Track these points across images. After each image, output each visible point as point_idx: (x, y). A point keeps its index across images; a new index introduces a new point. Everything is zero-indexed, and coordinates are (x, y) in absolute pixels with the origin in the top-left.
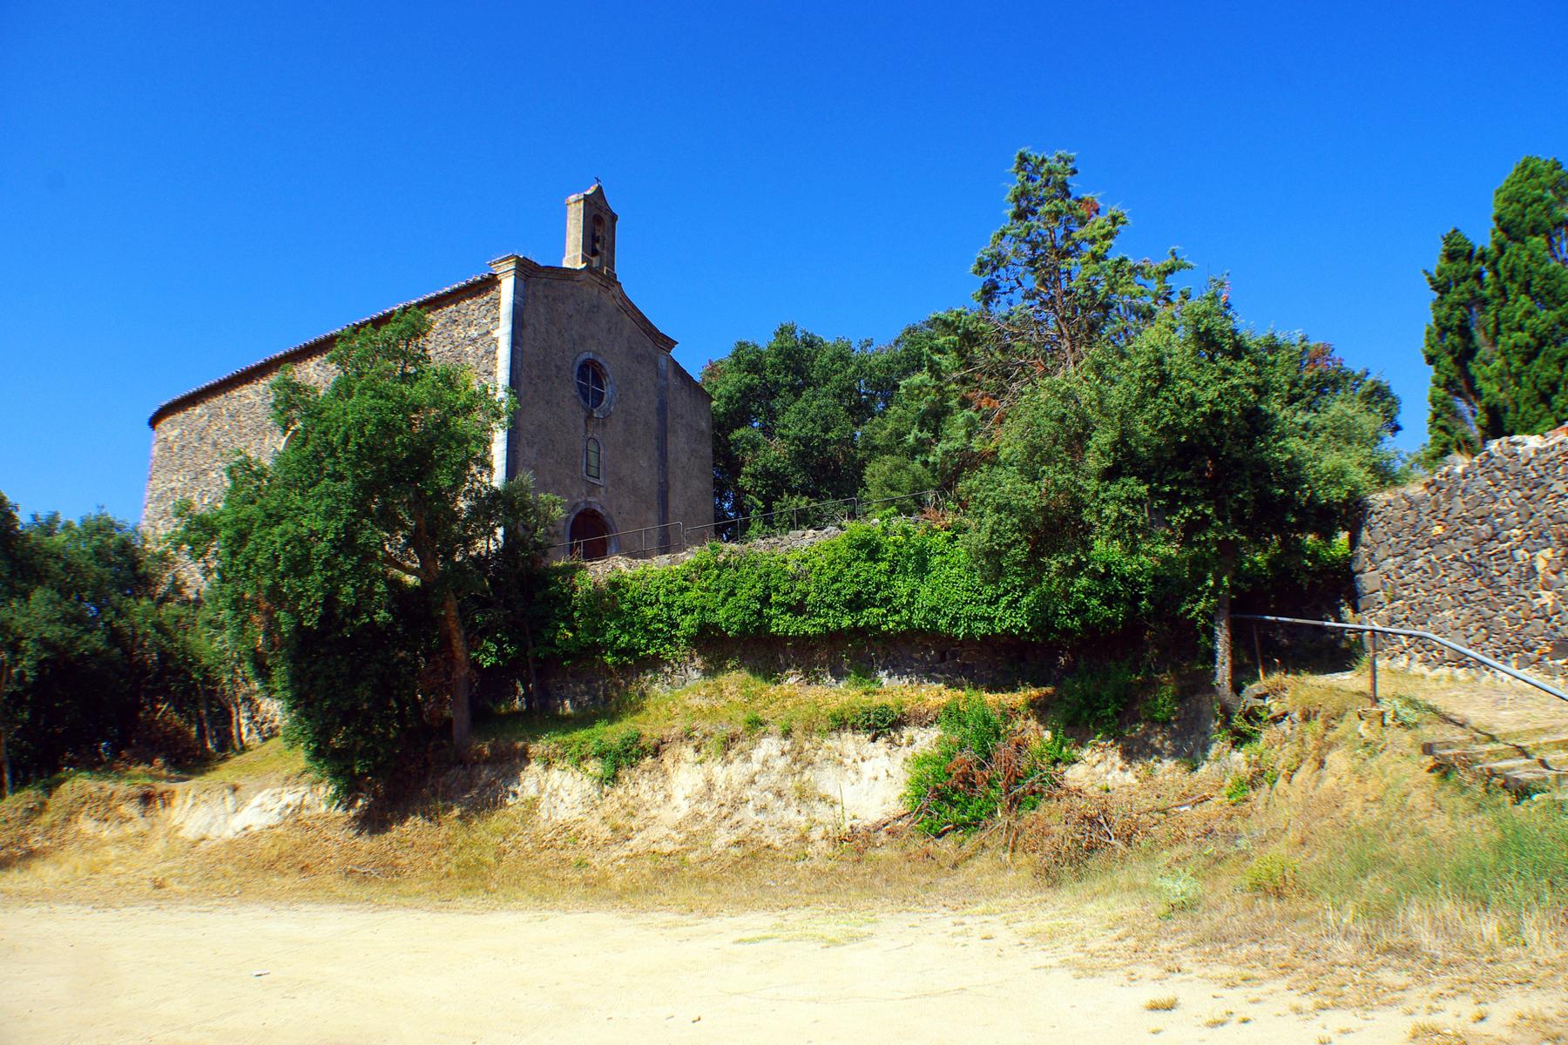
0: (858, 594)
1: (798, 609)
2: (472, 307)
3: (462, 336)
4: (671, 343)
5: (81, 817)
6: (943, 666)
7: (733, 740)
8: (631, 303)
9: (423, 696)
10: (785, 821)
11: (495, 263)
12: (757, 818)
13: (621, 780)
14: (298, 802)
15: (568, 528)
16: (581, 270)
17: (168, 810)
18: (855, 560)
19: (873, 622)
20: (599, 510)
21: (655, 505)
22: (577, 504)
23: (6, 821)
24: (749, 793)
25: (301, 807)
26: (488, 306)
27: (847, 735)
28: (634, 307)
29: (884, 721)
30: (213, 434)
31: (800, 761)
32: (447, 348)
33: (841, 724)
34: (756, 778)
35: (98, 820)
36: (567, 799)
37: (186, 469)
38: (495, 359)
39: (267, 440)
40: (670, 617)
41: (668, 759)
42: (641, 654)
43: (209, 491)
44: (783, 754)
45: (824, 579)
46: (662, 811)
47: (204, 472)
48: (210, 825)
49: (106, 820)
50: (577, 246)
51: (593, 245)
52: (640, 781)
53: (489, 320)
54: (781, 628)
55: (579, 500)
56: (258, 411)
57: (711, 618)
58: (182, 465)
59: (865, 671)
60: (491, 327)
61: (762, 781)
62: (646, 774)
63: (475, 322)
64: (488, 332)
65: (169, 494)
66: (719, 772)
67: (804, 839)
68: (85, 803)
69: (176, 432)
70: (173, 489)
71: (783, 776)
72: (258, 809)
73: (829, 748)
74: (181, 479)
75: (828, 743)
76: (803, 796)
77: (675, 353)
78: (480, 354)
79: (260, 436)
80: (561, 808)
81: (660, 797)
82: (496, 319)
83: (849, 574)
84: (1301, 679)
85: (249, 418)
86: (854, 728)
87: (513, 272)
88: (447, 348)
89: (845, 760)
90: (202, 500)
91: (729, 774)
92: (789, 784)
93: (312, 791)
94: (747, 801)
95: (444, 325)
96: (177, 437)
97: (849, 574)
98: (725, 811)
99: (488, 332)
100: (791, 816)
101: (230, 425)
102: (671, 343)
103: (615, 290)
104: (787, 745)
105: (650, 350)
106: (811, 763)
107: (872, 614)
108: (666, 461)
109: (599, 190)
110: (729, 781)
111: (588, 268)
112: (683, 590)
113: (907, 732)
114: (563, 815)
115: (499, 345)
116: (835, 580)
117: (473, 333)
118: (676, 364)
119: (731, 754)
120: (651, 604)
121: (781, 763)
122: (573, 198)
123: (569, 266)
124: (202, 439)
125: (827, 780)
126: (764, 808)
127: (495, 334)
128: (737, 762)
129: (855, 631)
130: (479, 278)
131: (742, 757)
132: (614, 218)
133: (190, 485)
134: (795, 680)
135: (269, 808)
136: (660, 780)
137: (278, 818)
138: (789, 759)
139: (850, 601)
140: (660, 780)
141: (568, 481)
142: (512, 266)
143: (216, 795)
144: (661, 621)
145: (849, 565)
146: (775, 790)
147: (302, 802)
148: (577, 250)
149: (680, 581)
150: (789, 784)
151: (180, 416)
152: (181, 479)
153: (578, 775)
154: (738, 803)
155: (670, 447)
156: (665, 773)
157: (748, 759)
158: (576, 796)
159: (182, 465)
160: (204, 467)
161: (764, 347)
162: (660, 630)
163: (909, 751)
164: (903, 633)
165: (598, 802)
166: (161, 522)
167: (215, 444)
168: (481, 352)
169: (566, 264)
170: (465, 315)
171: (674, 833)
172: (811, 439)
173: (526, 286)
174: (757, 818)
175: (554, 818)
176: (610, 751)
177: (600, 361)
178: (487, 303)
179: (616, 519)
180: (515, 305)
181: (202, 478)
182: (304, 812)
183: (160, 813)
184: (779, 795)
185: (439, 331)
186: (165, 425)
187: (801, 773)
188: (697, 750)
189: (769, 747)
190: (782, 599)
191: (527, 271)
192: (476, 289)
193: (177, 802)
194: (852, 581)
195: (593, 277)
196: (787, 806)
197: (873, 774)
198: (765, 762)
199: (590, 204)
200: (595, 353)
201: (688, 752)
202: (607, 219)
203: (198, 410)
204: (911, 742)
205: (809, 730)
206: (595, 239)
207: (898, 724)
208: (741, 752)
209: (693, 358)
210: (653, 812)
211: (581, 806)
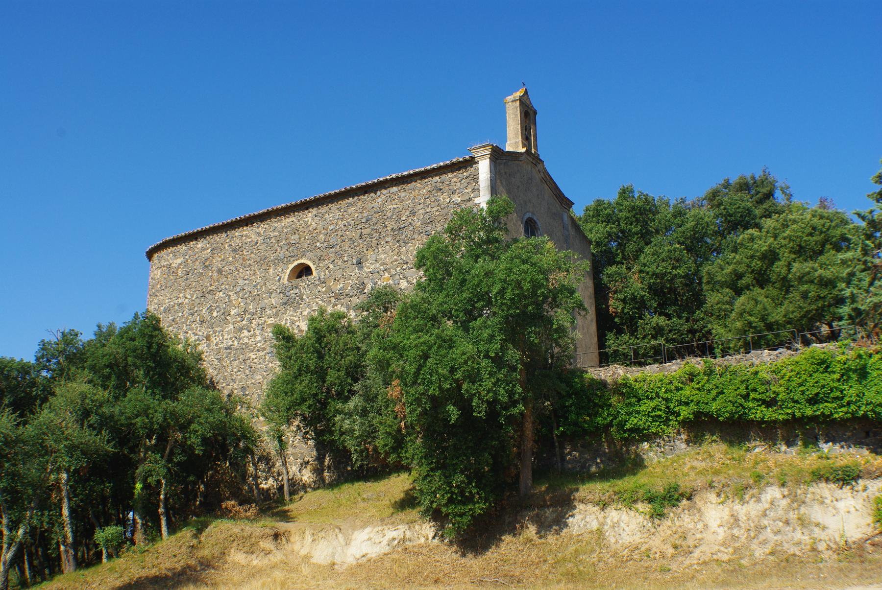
0: (817, 394)
1: (770, 403)
2: (454, 180)
3: (448, 201)
5: (233, 550)
6: (867, 441)
7: (746, 488)
8: (549, 175)
9: (212, 454)
10: (796, 539)
11: (474, 149)
12: (776, 538)
13: (667, 515)
14: (402, 536)
17: (290, 545)
18: (815, 372)
19: (827, 412)
23: (175, 556)
24: (765, 522)
25: (404, 540)
26: (468, 180)
27: (823, 485)
28: (551, 178)
29: (848, 476)
30: (217, 262)
31: (797, 501)
32: (435, 209)
33: (818, 476)
34: (768, 512)
35: (247, 553)
36: (626, 529)
37: (193, 290)
40: (668, 407)
41: (697, 499)
42: (645, 432)
43: (217, 307)
44: (784, 497)
45: (794, 384)
46: (704, 535)
48: (333, 554)
49: (253, 553)
50: (517, 134)
52: (682, 516)
53: (470, 190)
54: (757, 416)
56: (260, 248)
57: (705, 409)
58: (189, 286)
59: (811, 440)
60: (472, 195)
61: (772, 514)
62: (686, 512)
63: (458, 191)
64: (470, 199)
66: (742, 510)
67: (814, 549)
68: (233, 541)
69: (179, 261)
71: (787, 511)
72: (369, 542)
73: (813, 493)
74: (188, 296)
75: (811, 489)
76: (803, 522)
79: (264, 267)
80: (624, 535)
81: (700, 526)
82: (476, 190)
83: (811, 382)
85: (252, 253)
86: (827, 480)
87: (489, 156)
88: (435, 209)
89: (826, 501)
90: (211, 312)
91: (747, 510)
92: (793, 516)
93: (410, 528)
94: (766, 527)
95: (430, 192)
96: (180, 264)
97: (811, 382)
98: (752, 534)
99: (470, 199)
100: (798, 535)
101: (234, 258)
103: (540, 166)
104: (786, 491)
105: (559, 209)
106: (804, 502)
107: (825, 408)
109: (526, 92)
110: (748, 515)
112: (678, 389)
113: (861, 482)
114: (626, 539)
116: (800, 385)
119: (747, 497)
120: (652, 399)
121: (784, 503)
122: (509, 98)
123: (511, 150)
125: (816, 513)
126: (779, 531)
128: (752, 502)
129: (813, 419)
130: (461, 159)
131: (753, 499)
132: (535, 113)
133: (198, 301)
134: (761, 450)
135: (377, 541)
136: (697, 515)
137: (388, 547)
138: (789, 500)
139: (811, 399)
140: (697, 515)
142: (489, 152)
143: (330, 532)
144: (660, 410)
145: (811, 375)
146: (784, 519)
147: (404, 536)
148: (516, 137)
149: (676, 384)
150: (793, 516)
151: (182, 248)
152: (188, 296)
153: (632, 513)
154: (760, 529)
156: (699, 511)
157: (759, 500)
158: (633, 526)
160: (210, 288)
161: (612, 201)
162: (660, 416)
163: (865, 494)
164: (848, 419)
165: (654, 530)
169: (509, 148)
170: (449, 185)
171: (722, 549)
172: (665, 274)
173: (495, 167)
174: (776, 538)
175: (620, 542)
176: (657, 497)
177: (535, 218)
178: (467, 177)
180: (491, 180)
181: (210, 297)
182: (408, 543)
183: (286, 546)
184: (787, 523)
185: (427, 196)
186: (168, 255)
187: (798, 509)
188: (719, 495)
189: (773, 492)
190: (758, 397)
191: (498, 156)
192: (456, 167)
193: (295, 538)
194: (813, 386)
196: (794, 530)
197: (846, 510)
198: (772, 503)
200: (533, 213)
201: (712, 497)
202: (531, 113)
203: (200, 244)
204: (865, 489)
205: (798, 482)
207: (857, 478)
208: (753, 496)
210: (699, 536)
211: (639, 533)
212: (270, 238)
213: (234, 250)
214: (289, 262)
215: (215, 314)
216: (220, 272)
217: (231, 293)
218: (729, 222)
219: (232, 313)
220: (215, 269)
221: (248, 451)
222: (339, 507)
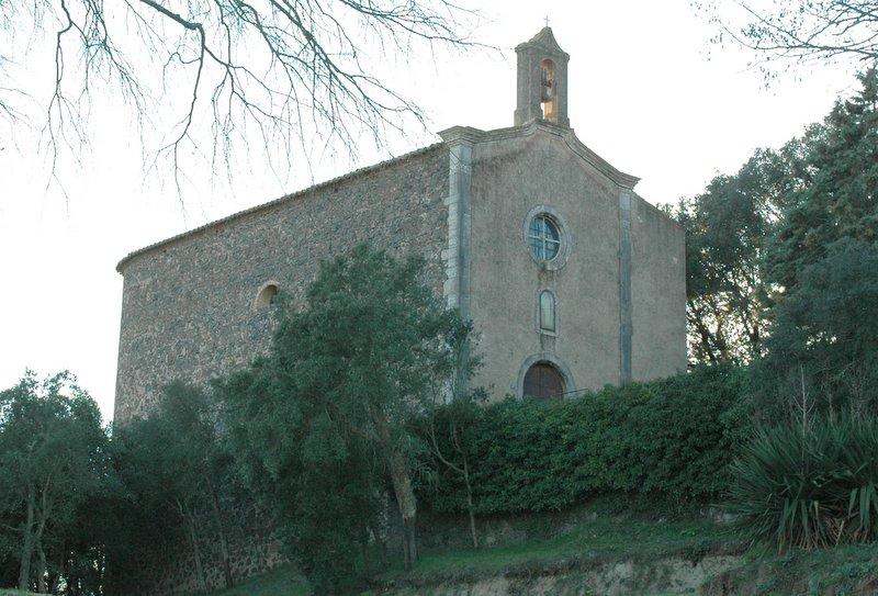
3: (417, 202)
4: (634, 181)
15: (522, 382)
21: (617, 351)
38: (447, 226)
43: (186, 343)
69: (148, 281)
77: (639, 190)
82: (446, 188)
90: (179, 351)
102: (634, 181)
103: (567, 137)
118: (641, 201)
124: (175, 290)
132: (566, 57)
141: (520, 336)
155: (634, 289)
166: (138, 372)
167: (189, 295)
179: (572, 368)
212: (240, 252)
213: (205, 268)
214: (259, 283)
215: (184, 352)
216: (189, 295)
217: (200, 326)
218: (812, 143)
219: (201, 350)
220: (184, 292)
221: (858, 110)
222: (301, 471)
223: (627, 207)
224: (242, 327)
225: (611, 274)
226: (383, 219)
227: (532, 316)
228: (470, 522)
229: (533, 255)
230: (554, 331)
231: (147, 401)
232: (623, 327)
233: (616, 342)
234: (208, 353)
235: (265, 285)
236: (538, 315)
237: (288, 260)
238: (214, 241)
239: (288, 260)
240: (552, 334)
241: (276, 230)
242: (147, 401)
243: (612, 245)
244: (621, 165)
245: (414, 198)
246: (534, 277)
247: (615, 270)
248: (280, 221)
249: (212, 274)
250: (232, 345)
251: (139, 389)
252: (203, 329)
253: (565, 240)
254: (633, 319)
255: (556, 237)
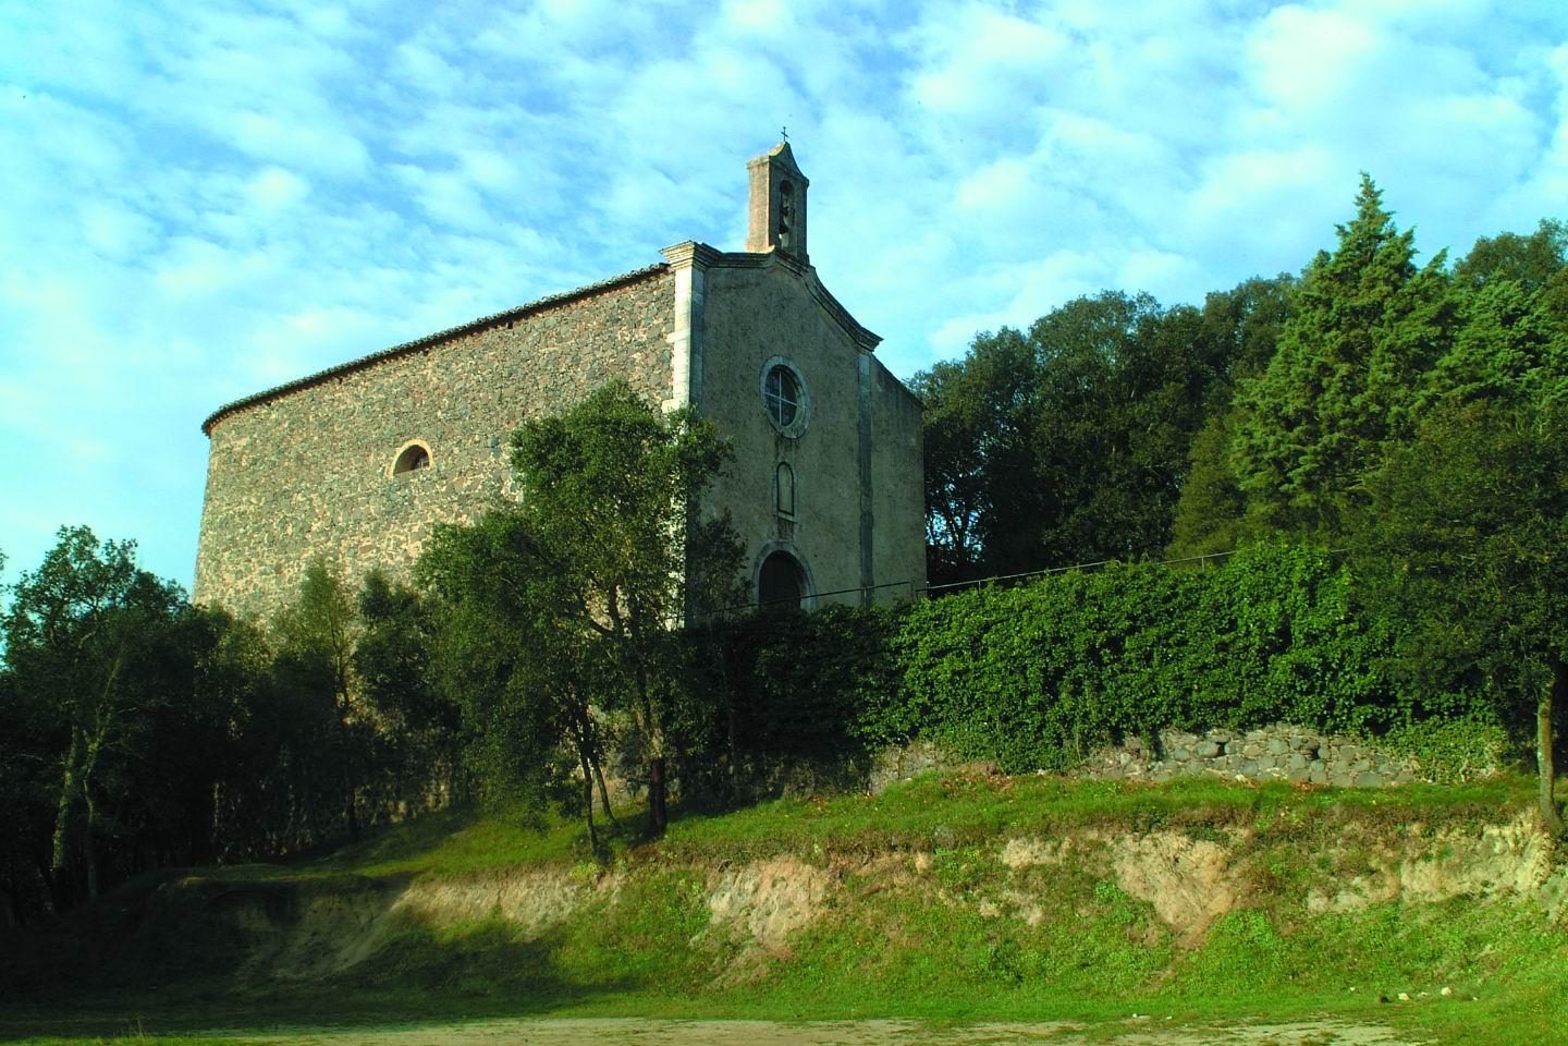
3: (628, 339)
4: (874, 340)
16: (769, 254)
20: (792, 552)
22: (767, 546)
30: (297, 446)
32: (609, 353)
38: (670, 369)
39: (372, 457)
47: (287, 494)
51: (782, 220)
55: (770, 541)
58: (255, 483)
64: (660, 336)
65: (237, 519)
69: (244, 442)
70: (241, 514)
78: (651, 364)
82: (669, 321)
84: (425, 1032)
90: (284, 528)
99: (660, 336)
102: (874, 340)
103: (807, 278)
108: (870, 490)
111: (779, 252)
115: (675, 352)
117: (641, 335)
127: (670, 338)
132: (805, 183)
142: (690, 254)
152: (254, 500)
155: (874, 470)
159: (255, 483)
166: (227, 554)
167: (300, 458)
168: (652, 361)
170: (630, 313)
181: (284, 502)
195: (782, 262)
199: (777, 167)
206: (783, 212)
209: (904, 359)
212: (372, 404)
214: (397, 444)
215: (290, 530)
216: (300, 458)
219: (314, 528)
220: (293, 455)
223: (867, 373)
224: (372, 499)
225: (851, 449)
226: (576, 362)
227: (769, 493)
228: (1533, 733)
229: (771, 416)
230: (793, 515)
231: (237, 592)
232: (863, 516)
233: (856, 536)
234: (323, 531)
235: (407, 445)
236: (775, 493)
237: (439, 413)
238: (336, 391)
239: (439, 413)
240: (791, 519)
241: (424, 377)
242: (237, 592)
243: (852, 416)
244: (865, 318)
245: (622, 334)
246: (771, 444)
247: (855, 444)
248: (430, 364)
249: (333, 431)
250: (357, 522)
251: (226, 576)
252: (317, 502)
253: (803, 404)
254: (875, 507)
255: (792, 397)
